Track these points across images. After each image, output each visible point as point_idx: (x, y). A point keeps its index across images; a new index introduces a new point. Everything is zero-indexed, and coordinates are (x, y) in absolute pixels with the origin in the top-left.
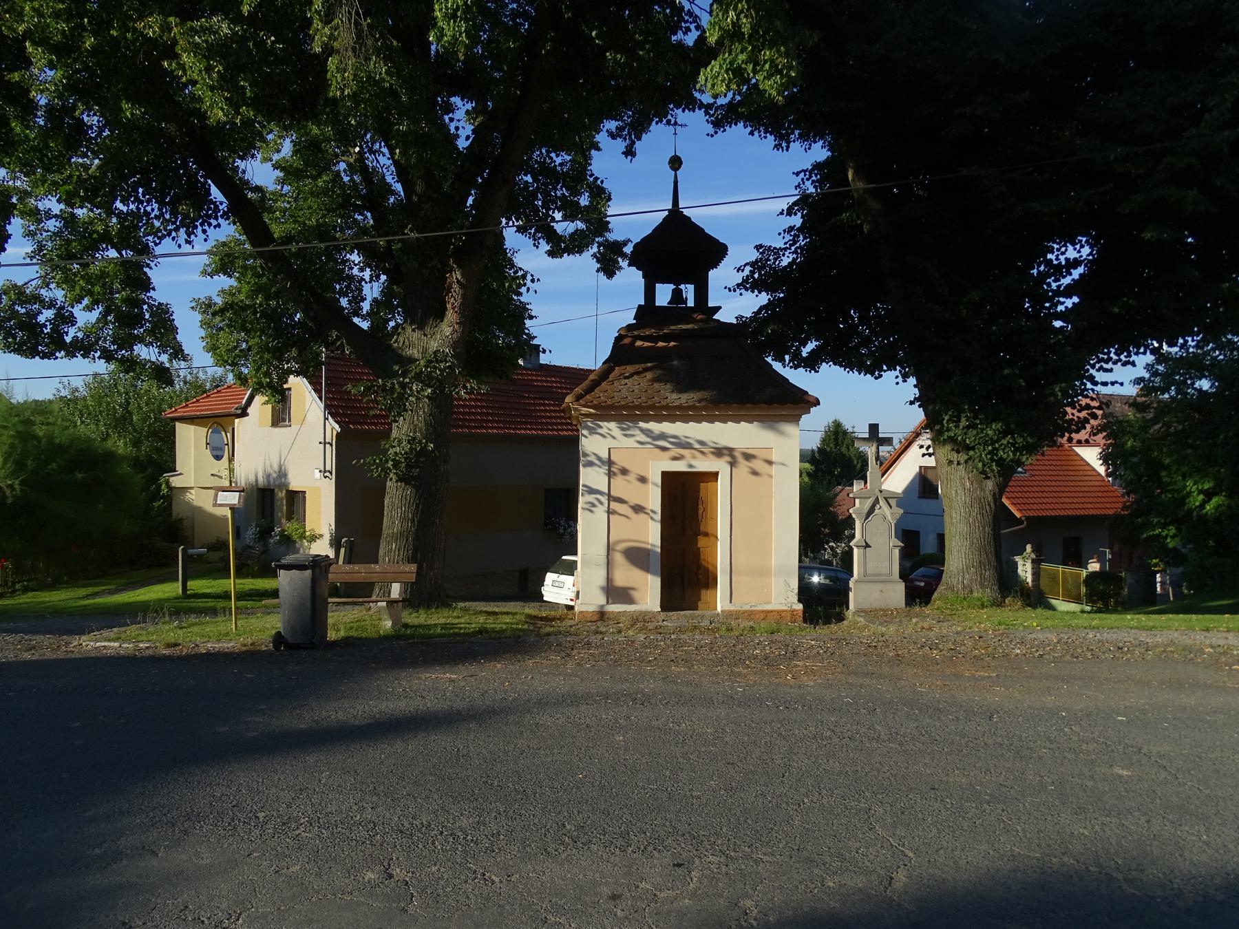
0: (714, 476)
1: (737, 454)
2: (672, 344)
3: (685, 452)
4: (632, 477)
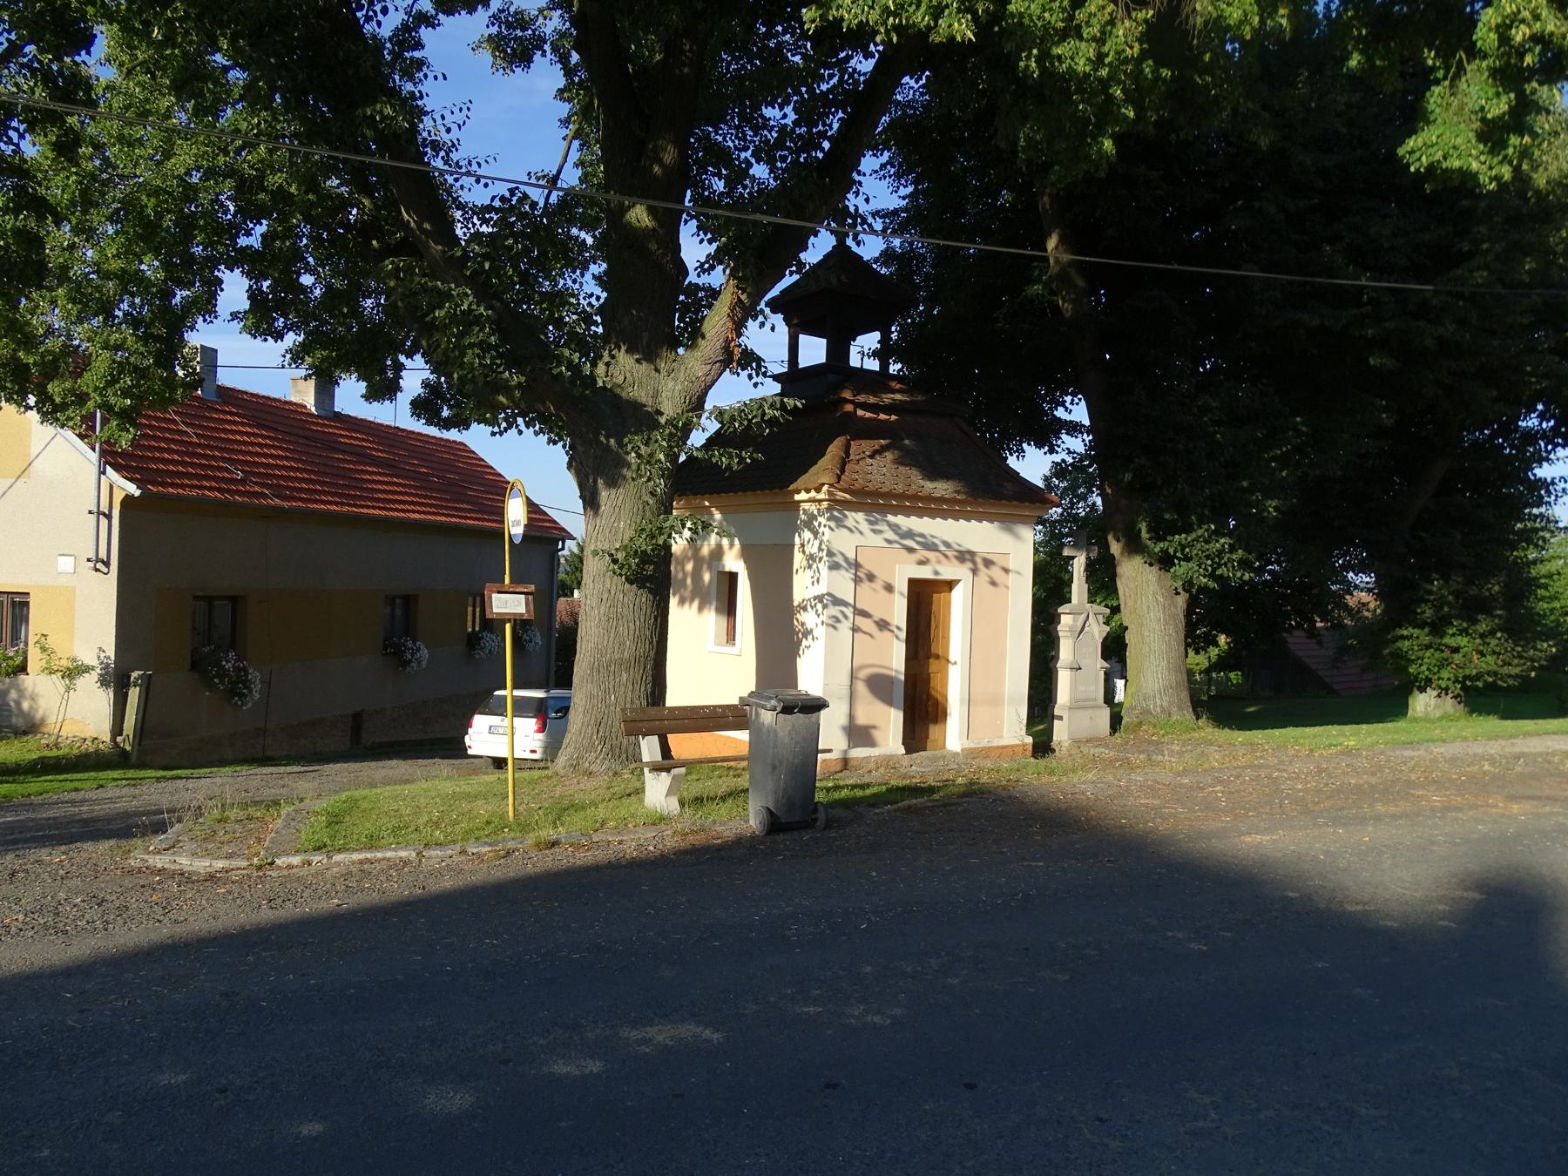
0: (950, 585)
1: (978, 560)
2: (894, 417)
3: (931, 555)
4: (878, 585)
